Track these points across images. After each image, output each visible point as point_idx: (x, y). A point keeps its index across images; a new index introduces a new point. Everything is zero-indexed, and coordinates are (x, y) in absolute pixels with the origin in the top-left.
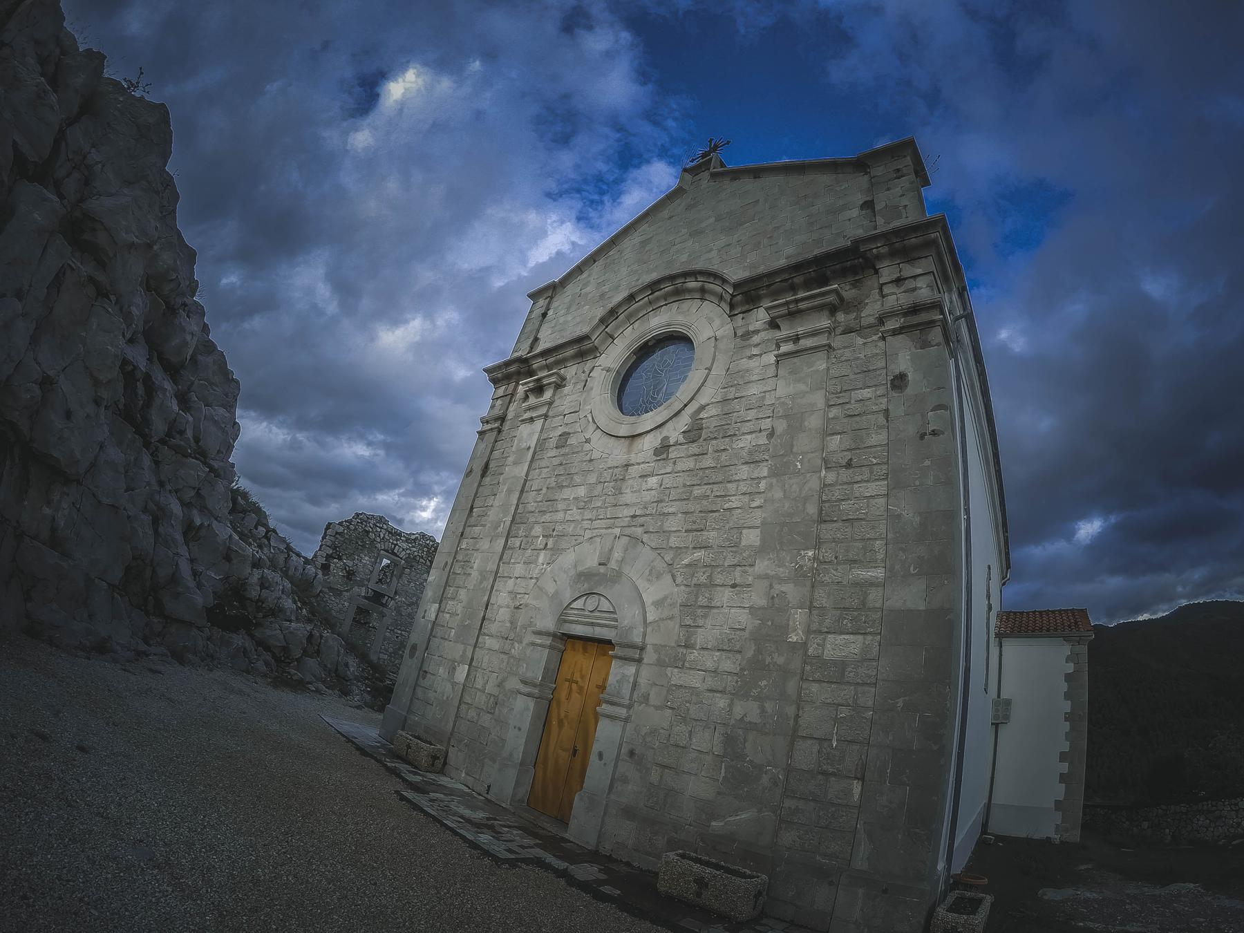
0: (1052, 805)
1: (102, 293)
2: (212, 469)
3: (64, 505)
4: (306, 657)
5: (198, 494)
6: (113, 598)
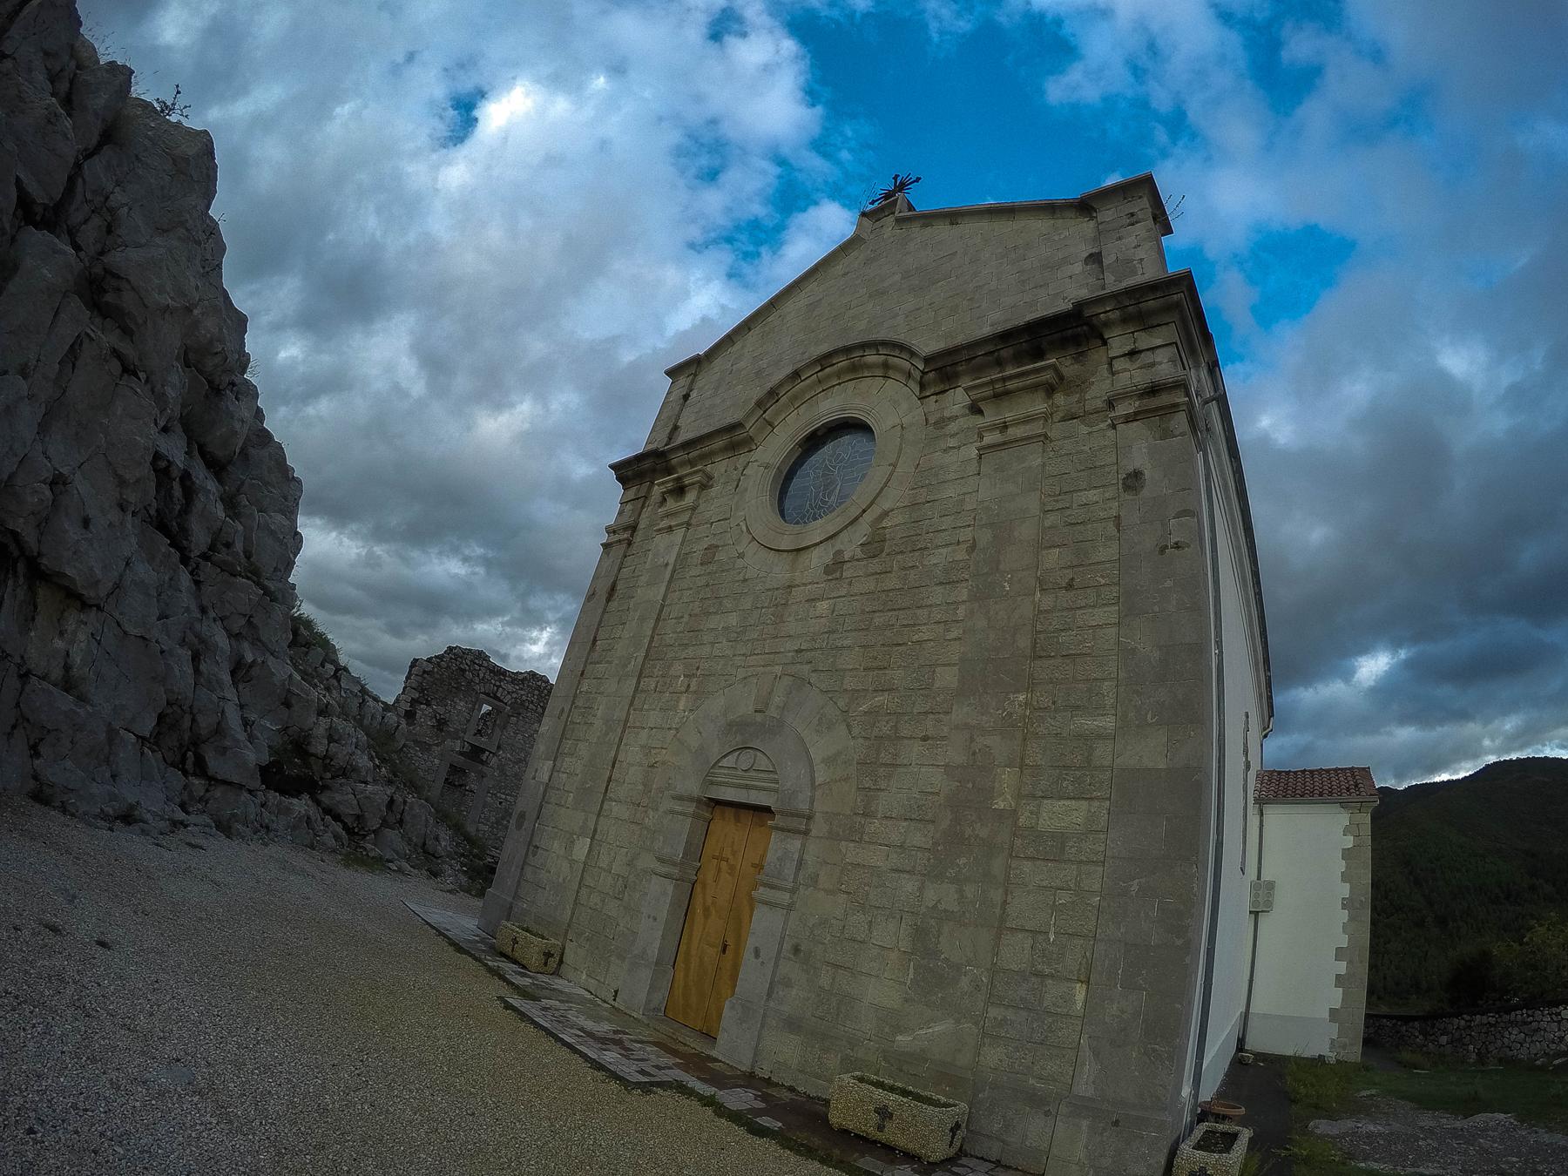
0: (1326, 1015)
6: (142, 753)
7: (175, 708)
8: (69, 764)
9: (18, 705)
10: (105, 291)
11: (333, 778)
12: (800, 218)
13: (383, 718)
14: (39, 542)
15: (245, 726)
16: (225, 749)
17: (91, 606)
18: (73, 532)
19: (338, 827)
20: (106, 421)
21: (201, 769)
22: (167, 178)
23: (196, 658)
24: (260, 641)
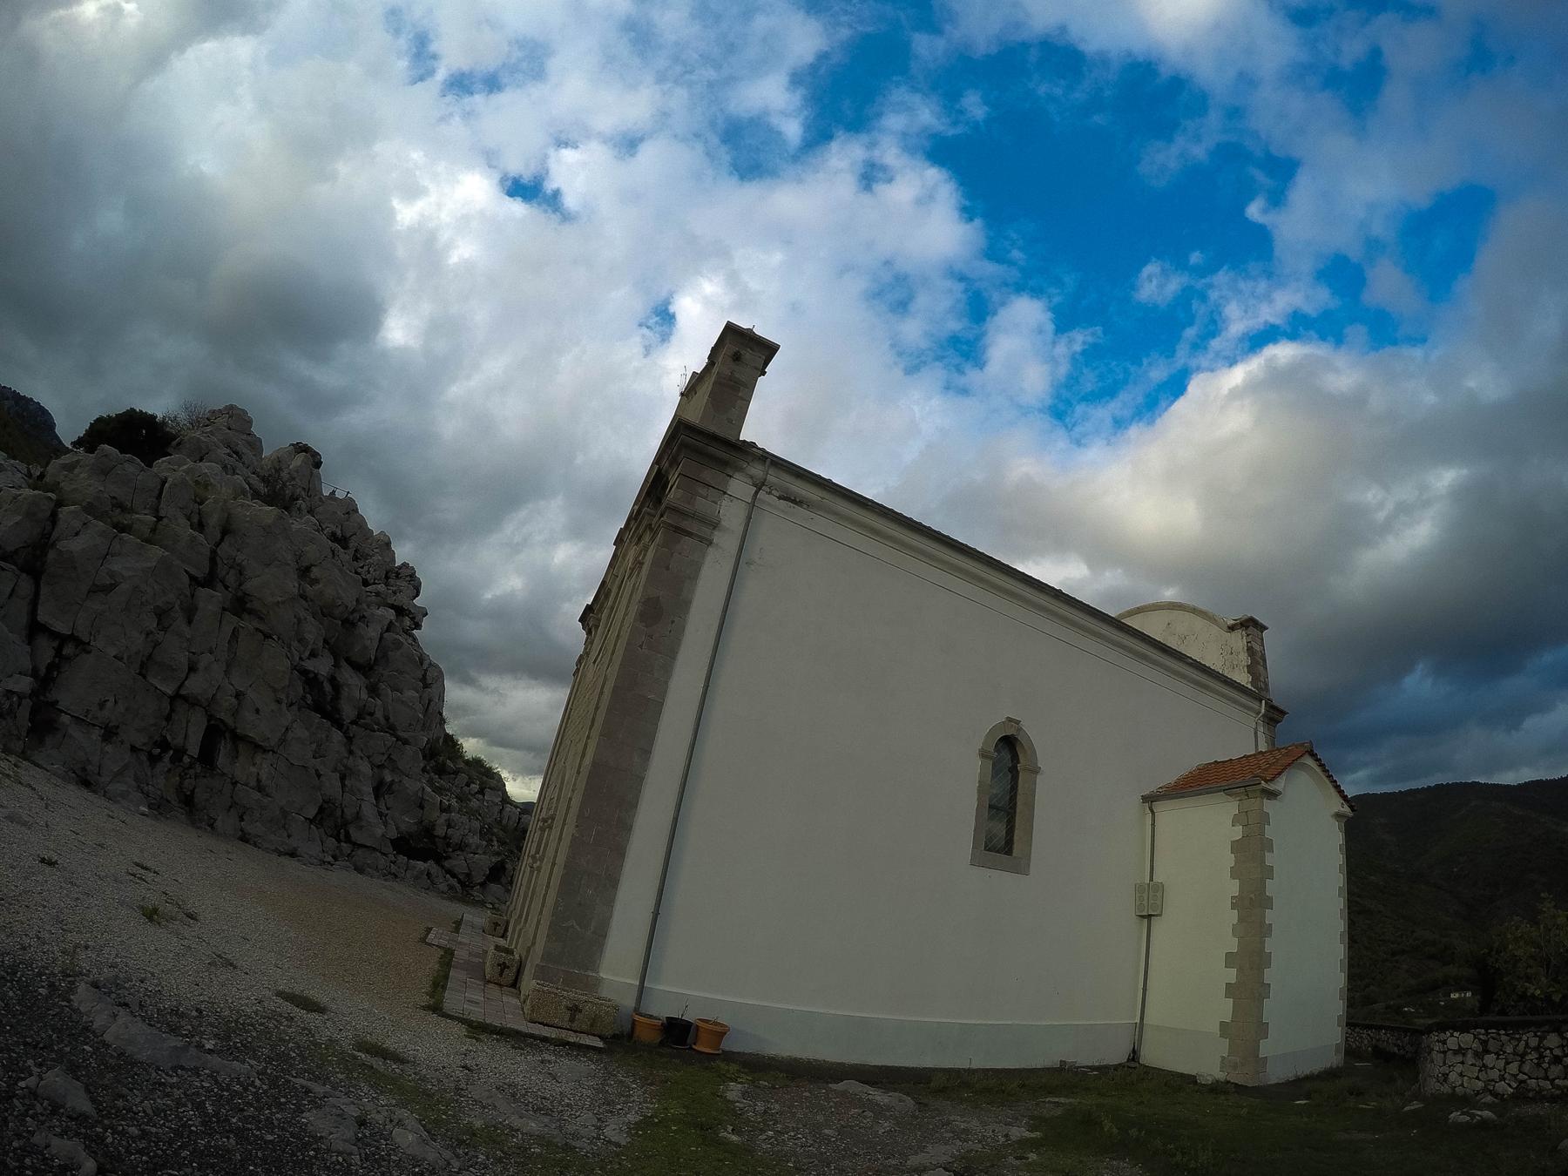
2: (399, 739)
6: (310, 828)
7: (331, 805)
9: (232, 797)
10: (247, 603)
11: (453, 851)
12: (993, 323)
14: (235, 722)
15: (381, 816)
16: (362, 827)
17: (269, 751)
19: (454, 882)
21: (348, 839)
23: (343, 778)
24: (399, 769)
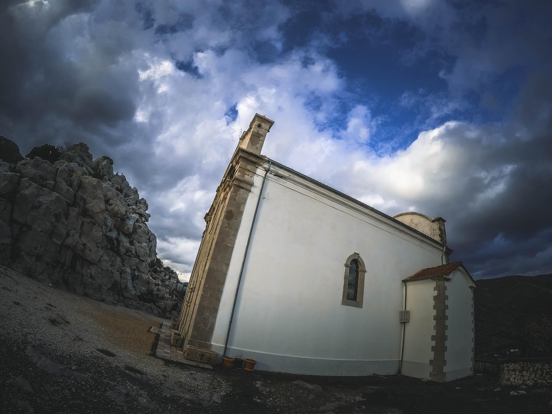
0: (428, 362)
1: (94, 224)
2: (140, 260)
3: (93, 270)
4: (173, 311)
5: (137, 267)
6: (109, 291)
8: (91, 290)
13: (183, 288)
18: (88, 252)
20: (91, 233)
22: (92, 190)
23: (121, 274)
